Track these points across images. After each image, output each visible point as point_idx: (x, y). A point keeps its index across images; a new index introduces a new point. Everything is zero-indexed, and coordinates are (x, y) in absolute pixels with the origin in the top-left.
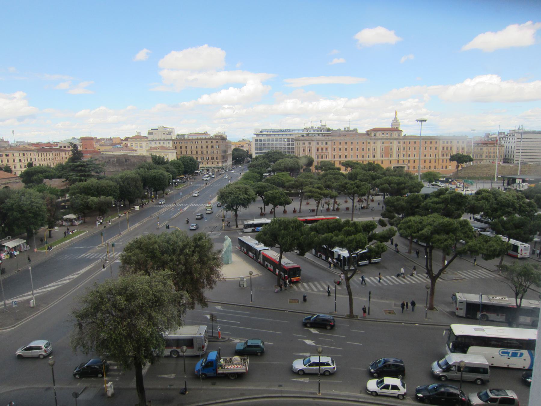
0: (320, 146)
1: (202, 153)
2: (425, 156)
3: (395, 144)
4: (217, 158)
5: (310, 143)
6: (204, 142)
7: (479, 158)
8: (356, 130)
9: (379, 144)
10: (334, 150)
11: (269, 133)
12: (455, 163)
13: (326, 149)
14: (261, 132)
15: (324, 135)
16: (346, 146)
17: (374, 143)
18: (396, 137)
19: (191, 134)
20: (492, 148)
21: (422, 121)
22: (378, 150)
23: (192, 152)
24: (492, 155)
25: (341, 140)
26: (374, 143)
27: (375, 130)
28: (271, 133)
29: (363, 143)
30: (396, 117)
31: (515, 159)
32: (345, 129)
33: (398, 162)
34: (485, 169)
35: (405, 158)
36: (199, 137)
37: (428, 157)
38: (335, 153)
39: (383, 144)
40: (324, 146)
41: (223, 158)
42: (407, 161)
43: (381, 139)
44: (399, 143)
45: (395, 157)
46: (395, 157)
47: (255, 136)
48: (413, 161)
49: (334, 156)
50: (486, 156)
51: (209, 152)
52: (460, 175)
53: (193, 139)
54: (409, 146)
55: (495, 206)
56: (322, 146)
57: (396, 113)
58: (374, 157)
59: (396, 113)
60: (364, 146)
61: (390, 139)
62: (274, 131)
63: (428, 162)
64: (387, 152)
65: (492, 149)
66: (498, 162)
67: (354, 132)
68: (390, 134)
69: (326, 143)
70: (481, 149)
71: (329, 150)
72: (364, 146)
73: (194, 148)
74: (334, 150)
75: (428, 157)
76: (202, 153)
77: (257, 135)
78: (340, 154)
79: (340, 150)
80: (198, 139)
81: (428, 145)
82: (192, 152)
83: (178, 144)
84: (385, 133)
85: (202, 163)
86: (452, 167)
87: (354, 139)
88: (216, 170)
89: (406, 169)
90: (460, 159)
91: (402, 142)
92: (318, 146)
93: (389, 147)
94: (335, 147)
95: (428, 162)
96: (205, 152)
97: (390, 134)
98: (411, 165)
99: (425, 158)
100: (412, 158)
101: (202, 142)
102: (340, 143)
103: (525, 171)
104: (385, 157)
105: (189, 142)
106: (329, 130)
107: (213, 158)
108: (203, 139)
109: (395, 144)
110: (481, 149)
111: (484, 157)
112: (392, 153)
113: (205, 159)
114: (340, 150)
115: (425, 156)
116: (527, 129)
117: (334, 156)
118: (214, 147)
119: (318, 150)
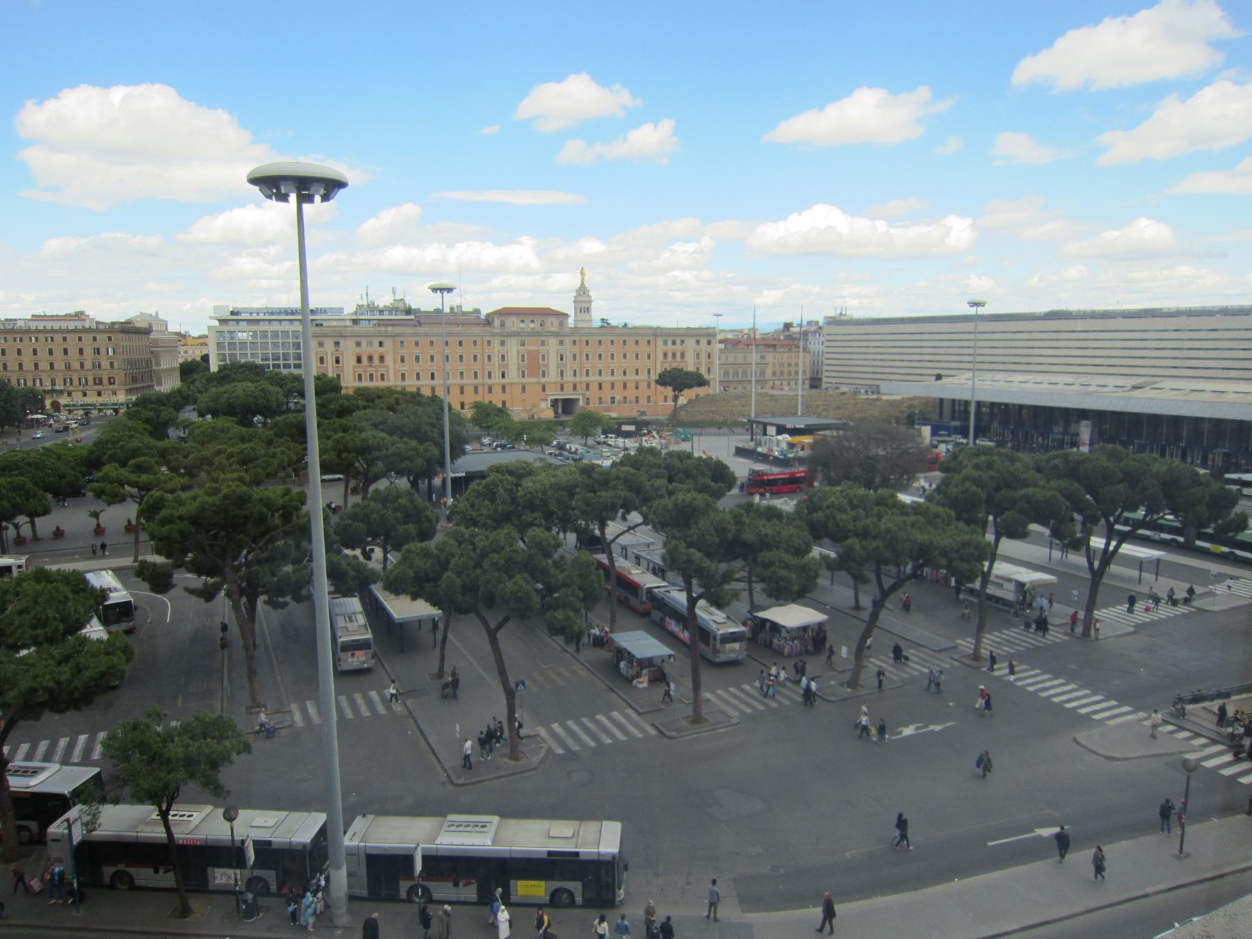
0: (365, 350)
1: (68, 367)
2: (625, 373)
3: (552, 346)
4: (111, 381)
5: (337, 344)
6: (58, 338)
7: (740, 378)
8: (477, 311)
9: (513, 347)
10: (403, 360)
11: (255, 317)
12: (669, 391)
13: (382, 359)
14: (232, 313)
15: (380, 323)
16: (431, 351)
17: (503, 343)
18: (555, 328)
19: (36, 318)
20: (785, 355)
21: (442, 290)
22: (513, 360)
23: (36, 366)
24: (786, 370)
25: (403, 335)
26: (503, 343)
27: (505, 313)
28: (262, 316)
29: (475, 343)
30: (582, 283)
31: (825, 380)
32: (452, 309)
33: (562, 389)
34: (737, 402)
35: (479, 380)
36: (56, 325)
37: (606, 378)
38: (404, 368)
39: (523, 344)
40: (375, 350)
41: (134, 380)
42: (584, 386)
43: (517, 334)
44: (561, 343)
45: (553, 376)
46: (553, 376)
47: (216, 323)
48: (571, 386)
49: (403, 375)
50: (774, 374)
51: (88, 365)
52: (682, 415)
53: (38, 331)
54: (587, 350)
55: (537, 502)
56: (370, 350)
57: (582, 273)
58: (503, 376)
59: (582, 273)
60: (477, 350)
61: (538, 334)
62: (272, 313)
63: (631, 386)
64: (533, 364)
65: (786, 358)
66: (800, 390)
67: (473, 317)
68: (538, 321)
69: (381, 344)
70: (762, 357)
71: (389, 360)
72: (477, 350)
73: (43, 356)
74: (403, 360)
75: (631, 377)
76: (68, 367)
77: (223, 321)
78: (418, 369)
79: (417, 359)
80: (53, 331)
81: (643, 349)
82: (36, 366)
83: (26, 342)
84: (528, 319)
85: (69, 394)
86: (662, 402)
87: (449, 334)
88: (109, 412)
89: (581, 403)
90: (676, 380)
91: (568, 341)
92: (358, 350)
93: (537, 352)
94: (403, 352)
95: (631, 386)
96: (76, 365)
97: (538, 321)
98: (593, 393)
99: (433, 383)
100: (594, 378)
101: (65, 339)
102: (417, 344)
103: (818, 406)
104: (530, 376)
105: (26, 337)
106: (409, 311)
107: (101, 380)
108: (68, 331)
109: (552, 346)
110: (762, 357)
111: (769, 374)
112: (547, 366)
113: (76, 382)
114: (417, 359)
115: (625, 373)
116: (857, 315)
117: (403, 375)
118: (103, 351)
119: (359, 360)
